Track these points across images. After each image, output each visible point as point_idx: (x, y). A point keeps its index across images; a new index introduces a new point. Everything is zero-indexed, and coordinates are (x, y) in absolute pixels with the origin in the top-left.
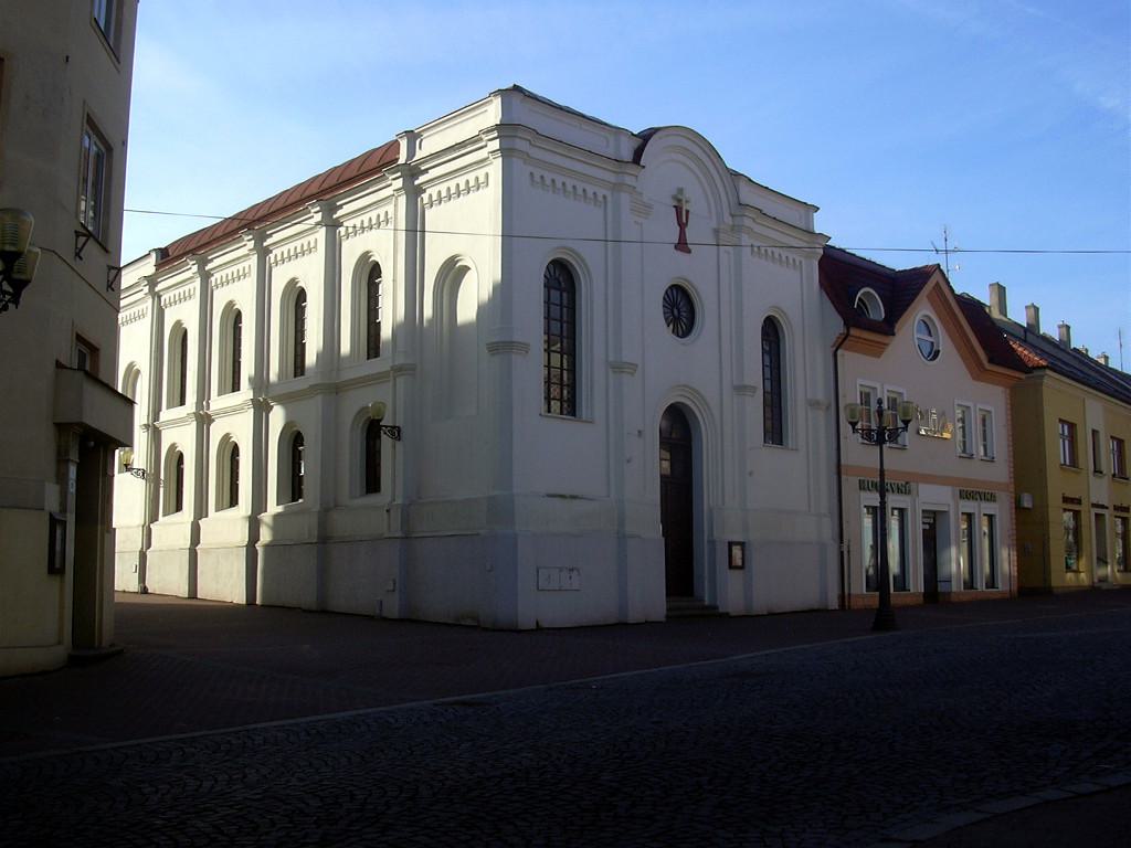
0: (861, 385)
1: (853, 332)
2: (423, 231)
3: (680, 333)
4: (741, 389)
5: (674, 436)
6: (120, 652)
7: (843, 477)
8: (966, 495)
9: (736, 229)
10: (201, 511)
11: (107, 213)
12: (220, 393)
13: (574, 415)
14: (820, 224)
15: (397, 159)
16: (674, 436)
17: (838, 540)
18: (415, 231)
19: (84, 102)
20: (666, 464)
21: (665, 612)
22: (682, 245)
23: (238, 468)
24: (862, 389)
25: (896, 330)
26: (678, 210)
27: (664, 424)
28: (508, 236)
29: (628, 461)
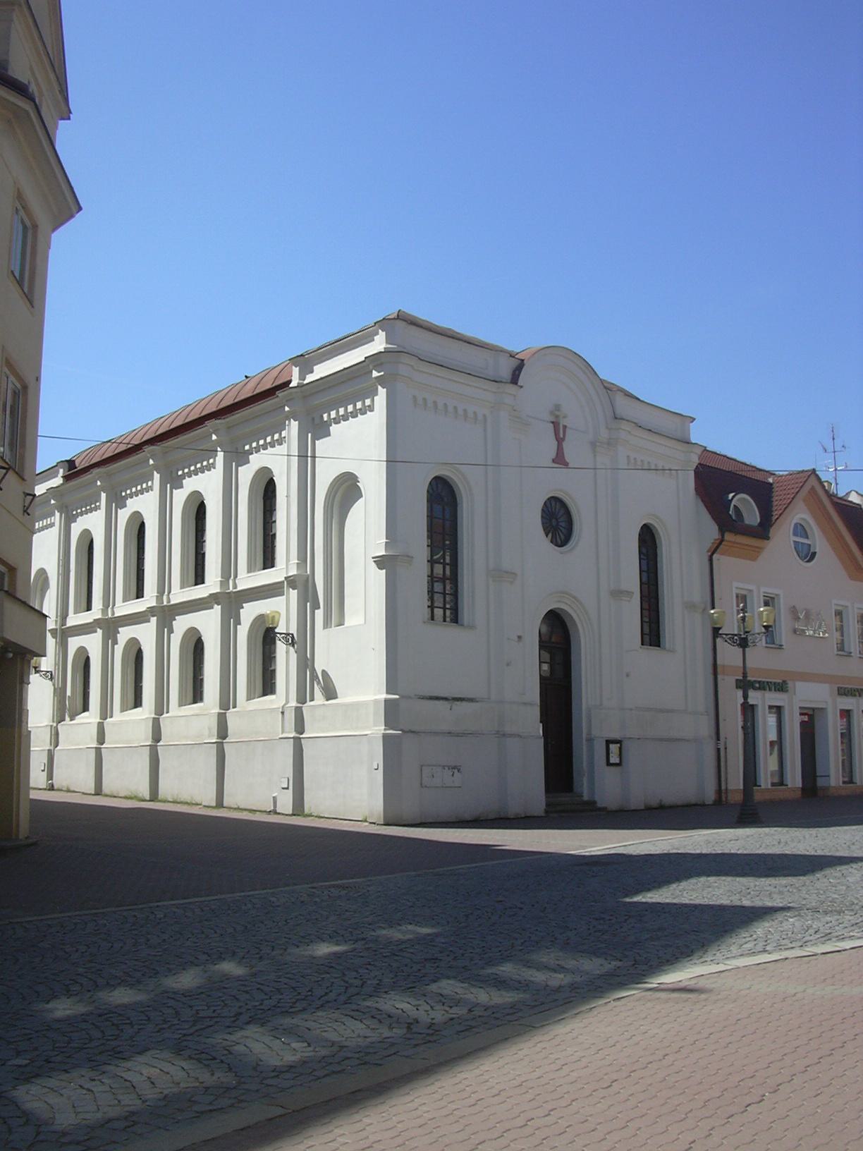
0: (737, 588)
1: (728, 536)
2: (314, 457)
3: (559, 542)
4: (618, 594)
5: (553, 640)
6: (35, 844)
7: (719, 677)
8: (843, 692)
9: (611, 443)
10: (105, 712)
11: (23, 445)
12: (125, 600)
13: (455, 619)
14: (698, 435)
15: (290, 381)
16: (553, 640)
17: (714, 737)
18: (306, 458)
19: (3, 347)
20: (545, 667)
21: (544, 807)
22: (560, 459)
23: (141, 694)
24: (739, 591)
25: (770, 535)
26: (556, 424)
27: (544, 629)
28: (392, 462)
29: (508, 665)
